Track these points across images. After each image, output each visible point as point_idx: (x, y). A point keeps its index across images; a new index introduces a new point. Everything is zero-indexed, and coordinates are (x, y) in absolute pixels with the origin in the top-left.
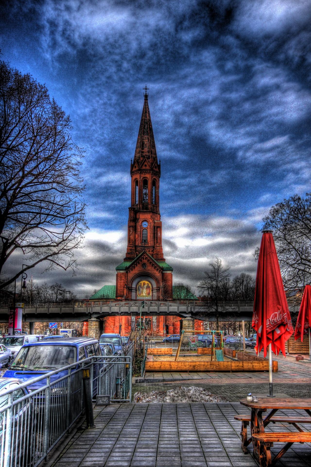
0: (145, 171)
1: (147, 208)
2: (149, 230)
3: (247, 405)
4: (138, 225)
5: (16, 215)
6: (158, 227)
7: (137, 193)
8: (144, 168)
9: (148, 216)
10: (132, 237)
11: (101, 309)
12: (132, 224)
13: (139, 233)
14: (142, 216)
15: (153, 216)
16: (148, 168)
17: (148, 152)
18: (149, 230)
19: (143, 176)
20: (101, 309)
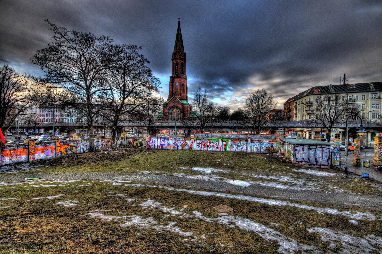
0: (178, 59)
1: (178, 76)
2: (179, 86)
3: (41, 143)
4: (174, 84)
5: (283, 197)
6: (183, 85)
7: (219, 195)
8: (177, 57)
9: (178, 80)
10: (171, 90)
11: (176, 124)
12: (171, 84)
13: (174, 88)
14: (176, 80)
15: (181, 80)
16: (178, 57)
17: (179, 49)
18: (179, 86)
19: (176, 61)
20: (176, 124)
